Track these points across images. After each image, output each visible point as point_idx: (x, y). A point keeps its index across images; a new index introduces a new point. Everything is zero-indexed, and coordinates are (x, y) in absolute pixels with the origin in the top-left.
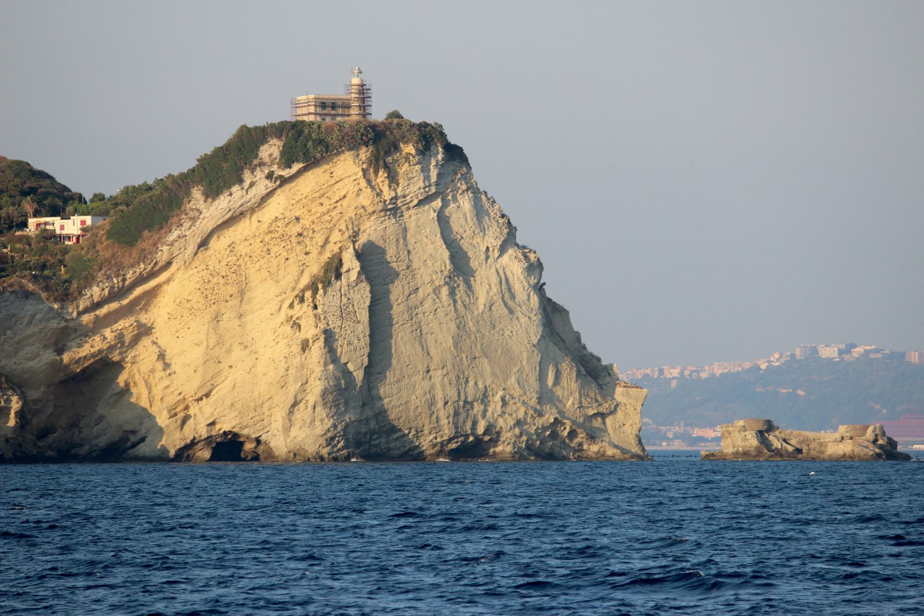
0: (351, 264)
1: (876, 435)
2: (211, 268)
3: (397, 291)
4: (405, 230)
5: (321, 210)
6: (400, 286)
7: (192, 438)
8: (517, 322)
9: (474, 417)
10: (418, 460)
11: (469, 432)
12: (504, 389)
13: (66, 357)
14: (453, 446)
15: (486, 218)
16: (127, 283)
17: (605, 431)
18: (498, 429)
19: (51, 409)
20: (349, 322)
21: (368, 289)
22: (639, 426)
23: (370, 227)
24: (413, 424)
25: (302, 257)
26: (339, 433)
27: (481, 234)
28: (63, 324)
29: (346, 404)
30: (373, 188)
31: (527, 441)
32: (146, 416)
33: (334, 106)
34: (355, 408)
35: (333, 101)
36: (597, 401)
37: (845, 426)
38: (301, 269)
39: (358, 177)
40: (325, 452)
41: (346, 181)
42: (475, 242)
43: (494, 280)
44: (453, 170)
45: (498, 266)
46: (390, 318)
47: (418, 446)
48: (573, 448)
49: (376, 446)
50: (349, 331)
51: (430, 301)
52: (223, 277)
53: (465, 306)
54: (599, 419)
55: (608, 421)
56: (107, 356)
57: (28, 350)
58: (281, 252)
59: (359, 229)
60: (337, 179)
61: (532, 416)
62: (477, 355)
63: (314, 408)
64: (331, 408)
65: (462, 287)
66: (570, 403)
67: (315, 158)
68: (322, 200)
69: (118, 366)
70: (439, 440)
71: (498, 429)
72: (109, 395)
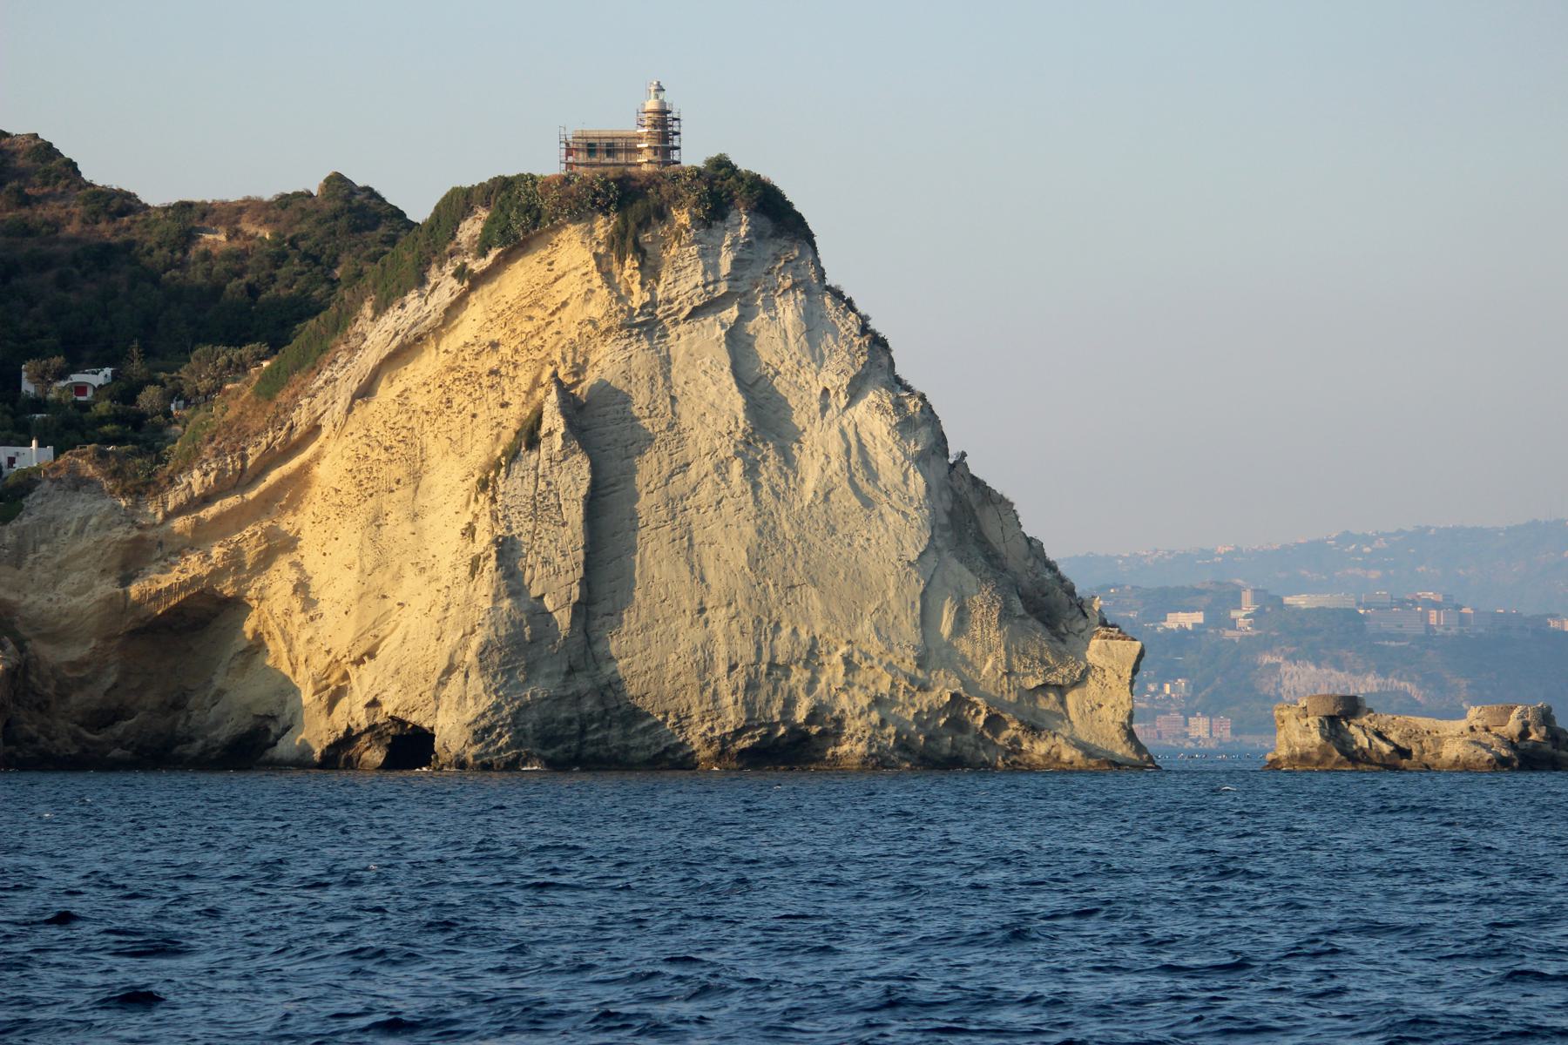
0: (553, 421)
1: (1526, 725)
3: (649, 469)
4: (667, 361)
5: (529, 327)
6: (655, 460)
7: (345, 727)
8: (879, 523)
9: (790, 691)
10: (684, 769)
11: (777, 718)
12: (849, 642)
13: (134, 590)
14: (744, 743)
15: (830, 338)
16: (250, 463)
17: (1064, 716)
19: (113, 679)
20: (546, 525)
21: (586, 466)
22: (1127, 708)
24: (670, 705)
26: (502, 719)
28: (135, 533)
29: (530, 669)
31: (898, 734)
34: (548, 676)
36: (1043, 662)
37: (1479, 708)
38: (495, 432)
39: (590, 269)
41: (571, 277)
42: (801, 380)
43: (836, 447)
45: (845, 422)
46: (634, 517)
47: (683, 744)
48: (1003, 747)
49: (596, 743)
50: (546, 541)
51: (709, 485)
54: (1052, 696)
55: (1072, 699)
57: (75, 577)
59: (586, 361)
60: (560, 273)
61: (907, 691)
62: (796, 582)
64: (494, 677)
65: (773, 460)
66: (989, 667)
69: (237, 606)
70: (717, 733)
71: (836, 713)
72: (231, 655)
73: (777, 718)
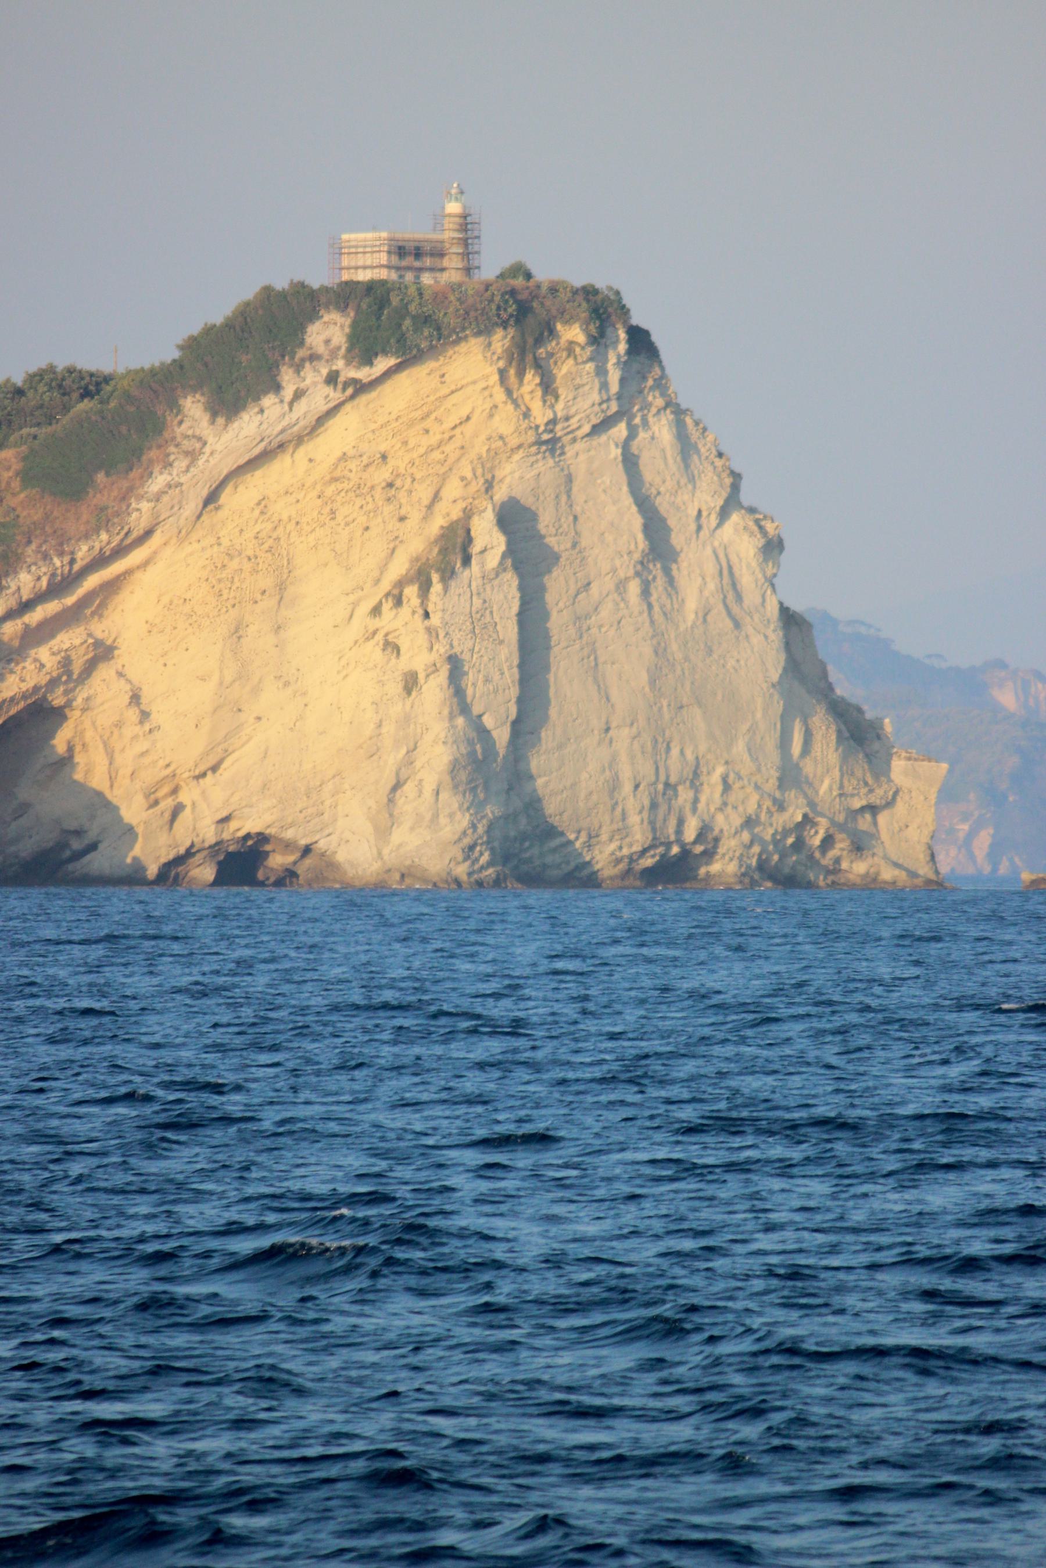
2: (225, 542)
4: (569, 479)
5: (426, 441)
7: (188, 844)
11: (672, 838)
12: (727, 763)
14: (648, 862)
17: (874, 836)
18: (716, 832)
21: (515, 583)
23: (512, 473)
25: (393, 524)
26: (481, 837)
27: (690, 487)
29: (486, 788)
30: (515, 403)
31: (760, 855)
32: (100, 803)
33: (418, 254)
35: (417, 244)
36: (866, 784)
38: (391, 546)
40: (461, 870)
41: (469, 390)
42: (679, 500)
43: (711, 568)
44: (639, 372)
45: (716, 544)
46: (547, 637)
47: (589, 863)
52: (249, 559)
53: (665, 614)
54: (868, 816)
55: (882, 818)
56: (44, 698)
58: (355, 515)
59: (493, 477)
60: (453, 387)
61: (769, 811)
62: (685, 701)
63: (438, 793)
65: (660, 582)
66: (825, 788)
67: (417, 346)
68: (428, 423)
69: (56, 715)
70: (625, 851)
71: (716, 832)
73: (672, 838)
